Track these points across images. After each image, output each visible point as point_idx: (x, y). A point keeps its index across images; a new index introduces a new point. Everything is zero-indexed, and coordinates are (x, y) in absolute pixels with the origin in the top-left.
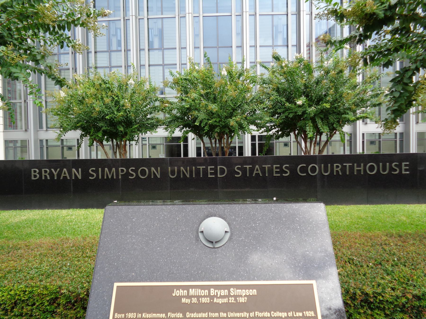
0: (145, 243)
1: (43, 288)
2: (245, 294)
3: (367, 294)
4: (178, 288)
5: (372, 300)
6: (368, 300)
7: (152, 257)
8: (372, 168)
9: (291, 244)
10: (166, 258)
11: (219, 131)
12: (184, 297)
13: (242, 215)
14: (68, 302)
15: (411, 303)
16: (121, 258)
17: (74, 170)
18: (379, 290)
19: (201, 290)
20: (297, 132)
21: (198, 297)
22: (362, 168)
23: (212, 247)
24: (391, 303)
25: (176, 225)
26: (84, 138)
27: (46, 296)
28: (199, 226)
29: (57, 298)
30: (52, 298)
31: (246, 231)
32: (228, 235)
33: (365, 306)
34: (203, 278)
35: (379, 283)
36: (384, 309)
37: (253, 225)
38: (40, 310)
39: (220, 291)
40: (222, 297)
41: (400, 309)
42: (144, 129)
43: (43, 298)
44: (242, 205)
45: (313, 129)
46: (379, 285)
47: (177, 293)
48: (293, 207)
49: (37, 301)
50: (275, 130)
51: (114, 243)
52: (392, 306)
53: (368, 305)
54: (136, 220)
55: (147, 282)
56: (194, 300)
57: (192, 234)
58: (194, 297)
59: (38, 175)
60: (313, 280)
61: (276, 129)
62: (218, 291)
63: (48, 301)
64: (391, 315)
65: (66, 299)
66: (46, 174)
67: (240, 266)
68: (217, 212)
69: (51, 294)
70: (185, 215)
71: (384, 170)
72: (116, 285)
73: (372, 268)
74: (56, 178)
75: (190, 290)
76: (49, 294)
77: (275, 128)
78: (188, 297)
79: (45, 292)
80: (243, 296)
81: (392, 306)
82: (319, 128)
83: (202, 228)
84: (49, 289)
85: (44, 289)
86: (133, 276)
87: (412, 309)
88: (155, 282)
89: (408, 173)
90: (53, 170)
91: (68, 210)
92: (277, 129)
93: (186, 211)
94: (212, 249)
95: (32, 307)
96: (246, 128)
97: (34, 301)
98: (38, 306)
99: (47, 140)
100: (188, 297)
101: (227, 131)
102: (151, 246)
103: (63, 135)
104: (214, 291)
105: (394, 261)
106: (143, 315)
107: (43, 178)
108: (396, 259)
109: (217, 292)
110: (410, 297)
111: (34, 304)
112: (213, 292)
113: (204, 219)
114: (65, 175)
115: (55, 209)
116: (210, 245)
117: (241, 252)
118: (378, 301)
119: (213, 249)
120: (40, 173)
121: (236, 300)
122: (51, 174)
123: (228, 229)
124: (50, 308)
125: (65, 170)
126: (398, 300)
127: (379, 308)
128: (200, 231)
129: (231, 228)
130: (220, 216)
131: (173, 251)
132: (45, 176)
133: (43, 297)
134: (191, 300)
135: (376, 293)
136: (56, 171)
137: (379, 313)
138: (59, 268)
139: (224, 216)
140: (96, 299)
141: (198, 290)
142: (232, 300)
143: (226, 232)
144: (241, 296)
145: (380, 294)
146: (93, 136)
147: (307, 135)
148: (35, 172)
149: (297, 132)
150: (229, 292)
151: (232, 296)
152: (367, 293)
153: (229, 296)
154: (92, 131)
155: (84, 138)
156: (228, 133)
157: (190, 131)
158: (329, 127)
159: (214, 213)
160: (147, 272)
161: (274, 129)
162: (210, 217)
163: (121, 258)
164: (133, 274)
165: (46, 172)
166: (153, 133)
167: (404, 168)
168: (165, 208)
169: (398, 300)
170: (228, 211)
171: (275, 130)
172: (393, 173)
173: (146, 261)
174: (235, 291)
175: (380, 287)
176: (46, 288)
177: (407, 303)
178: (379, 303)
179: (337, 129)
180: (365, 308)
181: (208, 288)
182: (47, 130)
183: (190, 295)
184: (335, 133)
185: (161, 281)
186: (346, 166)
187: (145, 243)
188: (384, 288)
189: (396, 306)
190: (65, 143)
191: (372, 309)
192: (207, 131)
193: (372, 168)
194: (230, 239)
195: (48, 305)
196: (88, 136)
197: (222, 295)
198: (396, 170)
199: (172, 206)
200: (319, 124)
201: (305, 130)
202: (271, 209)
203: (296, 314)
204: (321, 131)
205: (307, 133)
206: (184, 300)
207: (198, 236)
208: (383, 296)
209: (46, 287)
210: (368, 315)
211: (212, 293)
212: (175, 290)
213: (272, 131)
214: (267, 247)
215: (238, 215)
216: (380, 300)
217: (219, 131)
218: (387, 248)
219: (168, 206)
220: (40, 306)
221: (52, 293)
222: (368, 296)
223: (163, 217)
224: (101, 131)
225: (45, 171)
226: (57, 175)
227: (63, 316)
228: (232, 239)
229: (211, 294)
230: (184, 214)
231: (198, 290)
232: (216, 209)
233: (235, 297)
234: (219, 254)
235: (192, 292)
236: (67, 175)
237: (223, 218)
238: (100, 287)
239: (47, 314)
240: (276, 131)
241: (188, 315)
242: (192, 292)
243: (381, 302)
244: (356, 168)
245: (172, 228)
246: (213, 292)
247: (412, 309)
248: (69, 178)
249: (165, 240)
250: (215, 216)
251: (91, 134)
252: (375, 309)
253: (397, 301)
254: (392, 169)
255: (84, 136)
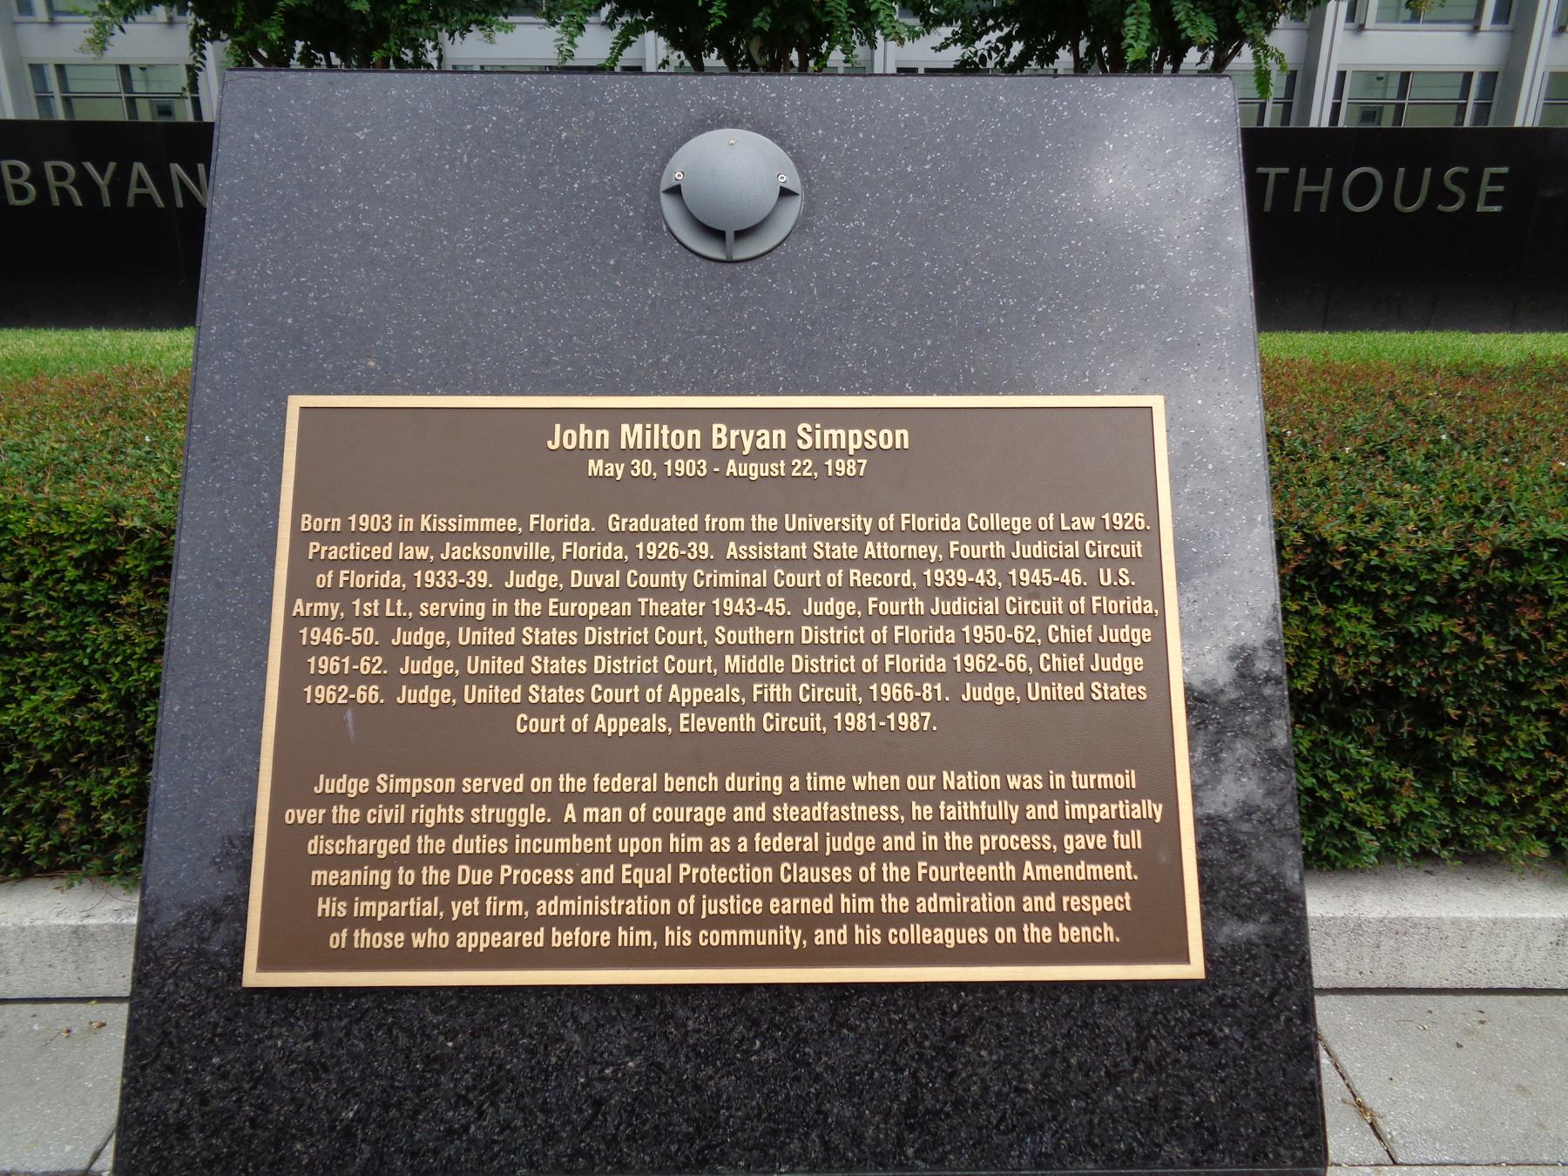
0: (419, 235)
1: (48, 513)
2: (859, 446)
3: (1322, 545)
4: (571, 417)
5: (1337, 565)
6: (1322, 568)
7: (454, 295)
8: (1363, 188)
9: (1072, 249)
10: (517, 302)
11: (766, 27)
12: (596, 453)
13: (858, 122)
14: (157, 568)
15: (1478, 573)
16: (315, 299)
17: (176, 169)
18: (1370, 532)
19: (671, 429)
20: (1083, 45)
21: (659, 455)
22: (1325, 188)
23: (721, 256)
24: (1410, 576)
25: (554, 164)
26: (208, 44)
27: (65, 544)
28: (663, 167)
29: (111, 555)
30: (92, 552)
31: (873, 195)
32: (794, 209)
33: (1308, 588)
34: (681, 383)
35: (1373, 507)
36: (1373, 600)
37: (909, 169)
38: (51, 598)
39: (752, 433)
40: (758, 455)
41: (1436, 598)
42: (457, 12)
43: (53, 554)
44: (861, 79)
45: (1153, 26)
46: (1371, 518)
47: (563, 438)
48: (1092, 91)
49: (34, 562)
50: (998, 34)
51: (273, 232)
52: (1410, 588)
53: (1318, 584)
54: (370, 134)
55: (434, 393)
56: (643, 467)
57: (629, 202)
58: (641, 453)
59: (31, 188)
60: (1154, 393)
61: (1001, 30)
62: (743, 433)
63: (77, 563)
64: (1399, 618)
65: (149, 559)
66: (66, 184)
67: (840, 339)
68: (743, 109)
69: (85, 537)
70: (596, 118)
71: (1408, 199)
72: (296, 403)
73: (1352, 463)
74: (107, 202)
75: (625, 428)
76: (78, 538)
77: (997, 26)
78: (615, 453)
79: (58, 528)
80: (851, 452)
81: (1410, 588)
82: (1179, 22)
83: (675, 173)
84: (74, 518)
85: (53, 517)
86: (369, 371)
87: (1480, 598)
88: (467, 395)
89: (1496, 209)
90: (89, 166)
91: (176, 332)
92: (1006, 30)
93: (602, 100)
94: (719, 265)
95: (18, 584)
96: (882, 16)
97: (22, 565)
98: (39, 581)
99: (60, 68)
100: (615, 453)
101: (802, 27)
102: (444, 247)
103: (116, 27)
104: (728, 435)
105: (1437, 442)
106: (424, 522)
107: (56, 200)
108: (1444, 437)
109: (739, 437)
110: (1483, 552)
111: (23, 575)
112: (721, 435)
113: (686, 139)
114: (142, 191)
115: (125, 329)
116: (710, 249)
117: (849, 279)
118: (1360, 568)
119: (726, 267)
120: (38, 179)
121: (820, 466)
122: (84, 182)
123: (791, 179)
124: (91, 592)
125: (139, 167)
126: (1435, 566)
127: (1359, 596)
128: (665, 185)
129: (806, 181)
130: (758, 128)
131: (546, 272)
132: (63, 192)
133: (53, 549)
134: (630, 467)
135: (1357, 541)
136: (102, 173)
137: (1354, 610)
138: (110, 452)
139: (776, 125)
140: (214, 460)
141: (657, 427)
142: (804, 467)
143: (785, 193)
144: (843, 453)
145: (1370, 545)
146: (242, 34)
147: (1124, 52)
148: (16, 172)
149: (1083, 45)
150: (793, 436)
151: (803, 453)
152: (1324, 541)
153: (791, 451)
154: (240, 12)
155: (208, 44)
156: (807, 39)
157: (651, 26)
158: (1218, 22)
159: (733, 112)
160: (431, 356)
161: (993, 28)
162: (711, 128)
163: (315, 299)
164: (372, 364)
165: (61, 174)
166: (499, 36)
167: (1485, 188)
168: (504, 87)
169: (1435, 566)
170: (794, 103)
171: (998, 34)
172: (1440, 207)
173: (425, 314)
174: (818, 433)
175: (1377, 522)
176: (58, 512)
177: (1465, 577)
178: (1361, 577)
179: (1249, 32)
180: (1307, 595)
181: (703, 418)
182: (52, 23)
183: (623, 446)
184: (1237, 49)
185: (495, 393)
186: (1266, 176)
187: (419, 235)
188: (1390, 525)
189: (1424, 587)
190: (138, 87)
191: (1330, 601)
192: (719, 22)
193: (1363, 188)
194: (804, 226)
195: (82, 580)
196: (224, 36)
197: (760, 446)
198: (1456, 178)
199: (535, 77)
200: (1180, 7)
201: (1119, 32)
202: (994, 99)
203: (1069, 522)
204: (1183, 36)
205: (1124, 45)
206: (595, 467)
207: (659, 214)
208: (1382, 554)
209: (59, 510)
210: (1311, 619)
211: (720, 440)
212: (558, 427)
213: (985, 38)
214: (966, 263)
215: (843, 122)
216: (1368, 567)
217: (766, 27)
218: (1414, 405)
219: (517, 78)
220: (50, 583)
221: (86, 535)
222: (1325, 552)
223: (495, 123)
224: (277, 17)
225: (55, 168)
226: (111, 187)
227: (146, 621)
228: (811, 225)
229: (715, 445)
230: (591, 114)
231: (657, 427)
232: (741, 96)
233: (819, 454)
234: (750, 290)
235: (631, 435)
236: (152, 189)
237: (772, 136)
238: (230, 414)
239: (83, 613)
240: (1000, 40)
241: (617, 524)
242: (631, 435)
243: (1372, 572)
244: (1302, 188)
245: (541, 173)
246: (721, 435)
247: (1480, 598)
248: (160, 203)
249: (508, 224)
250: (736, 124)
251: (237, 24)
252: (1343, 599)
253: (1432, 570)
254: (1439, 193)
255: (205, 37)
